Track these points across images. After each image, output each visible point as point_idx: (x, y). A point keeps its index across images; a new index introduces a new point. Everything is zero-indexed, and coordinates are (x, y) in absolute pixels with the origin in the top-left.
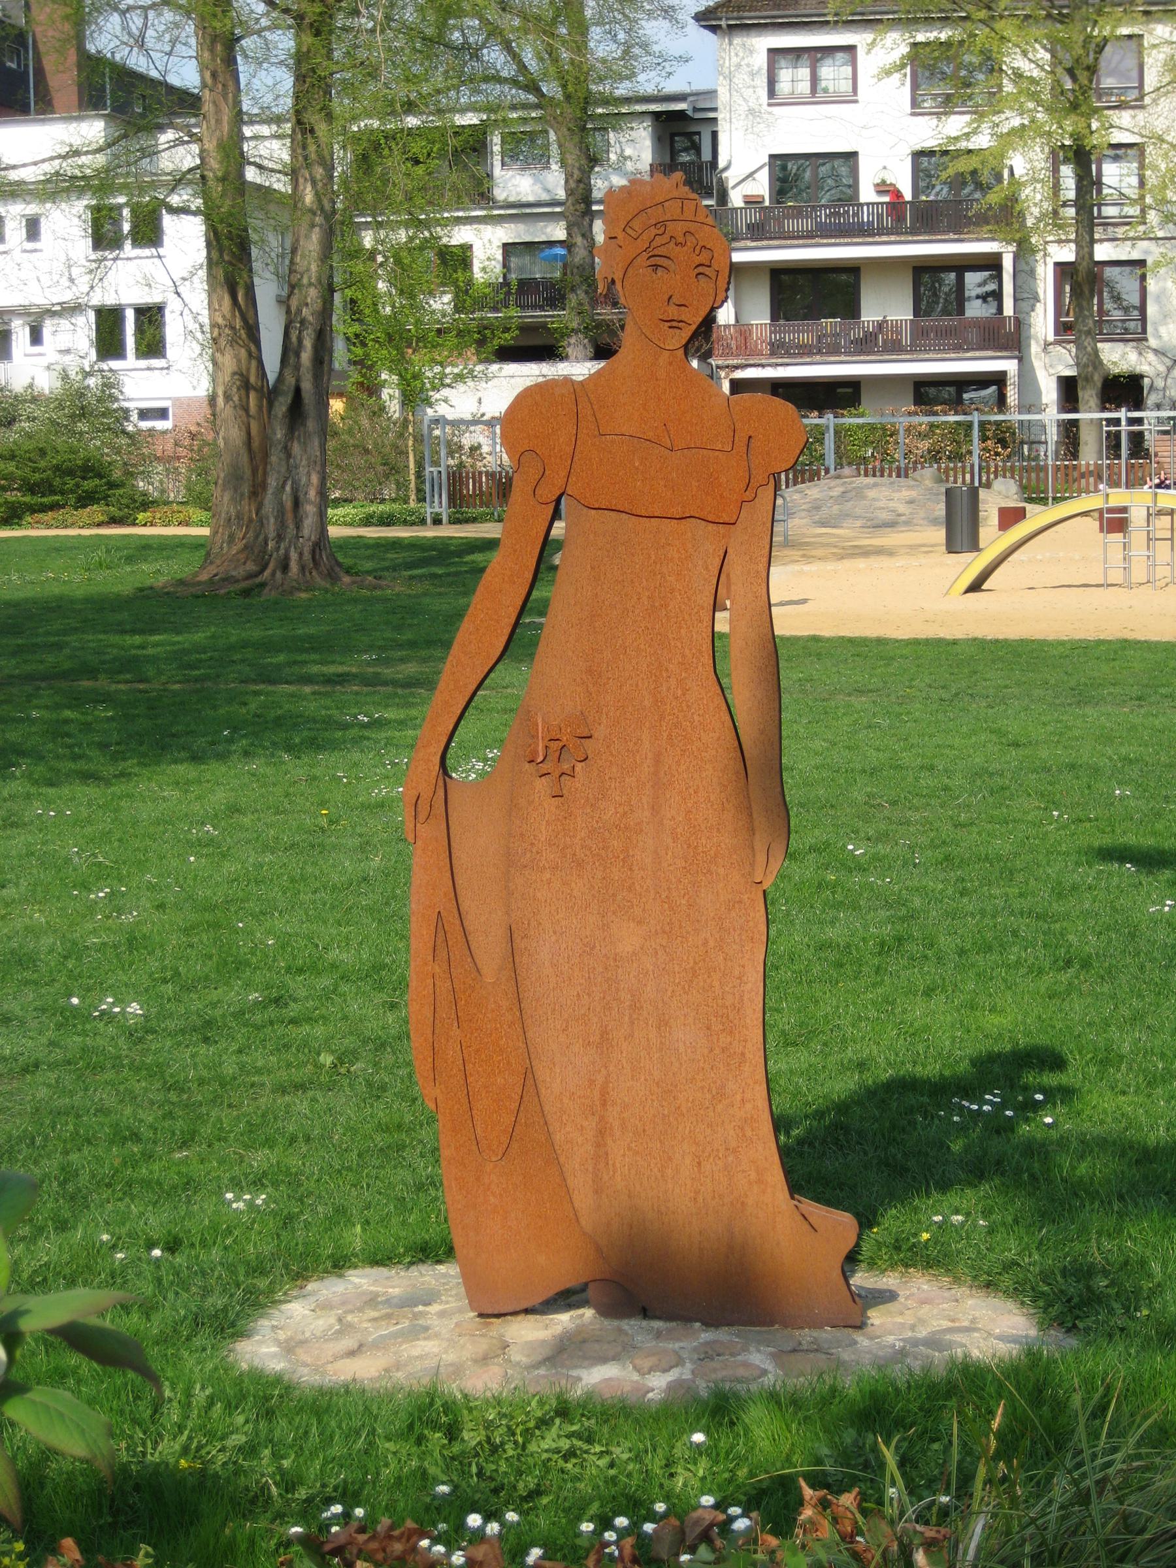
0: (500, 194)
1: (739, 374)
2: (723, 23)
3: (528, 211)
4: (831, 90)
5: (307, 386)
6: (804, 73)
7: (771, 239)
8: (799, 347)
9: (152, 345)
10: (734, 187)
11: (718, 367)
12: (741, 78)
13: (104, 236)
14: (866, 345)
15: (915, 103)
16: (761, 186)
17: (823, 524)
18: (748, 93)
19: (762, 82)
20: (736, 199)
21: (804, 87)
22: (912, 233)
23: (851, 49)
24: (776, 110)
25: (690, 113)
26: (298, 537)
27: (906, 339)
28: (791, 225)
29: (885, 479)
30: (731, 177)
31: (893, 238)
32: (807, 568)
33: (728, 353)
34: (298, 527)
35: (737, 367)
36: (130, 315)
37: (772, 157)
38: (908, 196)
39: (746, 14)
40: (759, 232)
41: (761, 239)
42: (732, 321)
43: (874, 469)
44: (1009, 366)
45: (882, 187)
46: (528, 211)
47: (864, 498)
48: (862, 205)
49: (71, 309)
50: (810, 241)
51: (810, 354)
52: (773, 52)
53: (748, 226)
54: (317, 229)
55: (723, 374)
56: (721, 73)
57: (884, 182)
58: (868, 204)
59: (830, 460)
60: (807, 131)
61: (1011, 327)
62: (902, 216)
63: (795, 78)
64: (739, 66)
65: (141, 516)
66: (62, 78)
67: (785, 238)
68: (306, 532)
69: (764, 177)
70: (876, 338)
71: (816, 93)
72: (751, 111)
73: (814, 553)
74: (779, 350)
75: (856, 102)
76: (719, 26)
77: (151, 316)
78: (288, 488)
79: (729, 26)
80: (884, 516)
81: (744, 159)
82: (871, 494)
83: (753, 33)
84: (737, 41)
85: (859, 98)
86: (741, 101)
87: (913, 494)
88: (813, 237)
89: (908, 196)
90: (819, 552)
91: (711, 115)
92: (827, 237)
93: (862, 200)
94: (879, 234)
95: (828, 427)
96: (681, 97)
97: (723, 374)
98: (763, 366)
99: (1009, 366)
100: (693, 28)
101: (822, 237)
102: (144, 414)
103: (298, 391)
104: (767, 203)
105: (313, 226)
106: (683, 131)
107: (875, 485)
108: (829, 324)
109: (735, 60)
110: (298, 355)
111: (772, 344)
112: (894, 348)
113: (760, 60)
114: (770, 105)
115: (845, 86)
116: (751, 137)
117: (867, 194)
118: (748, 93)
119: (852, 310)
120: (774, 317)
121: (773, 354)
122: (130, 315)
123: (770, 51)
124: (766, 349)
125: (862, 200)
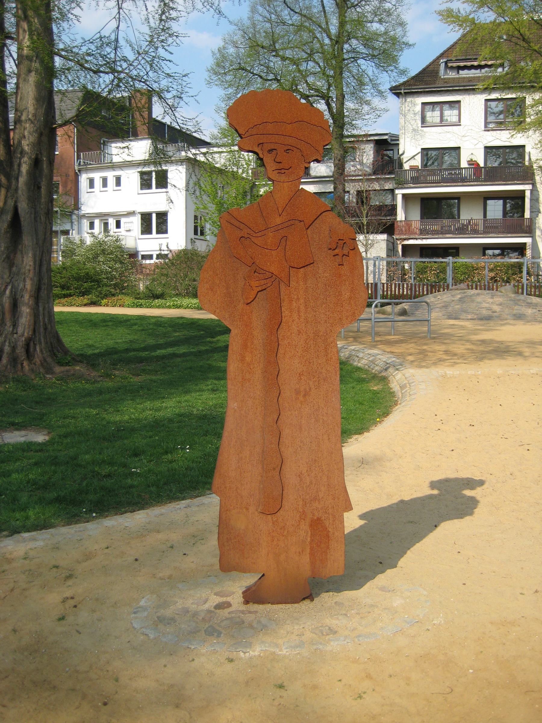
0: (313, 173)
1: (406, 242)
2: (402, 91)
3: (324, 179)
4: (449, 120)
5: (23, 206)
6: (437, 113)
7: (421, 183)
8: (433, 231)
9: (162, 228)
10: (405, 163)
11: (397, 239)
12: (410, 116)
13: (145, 184)
14: (462, 231)
15: (486, 123)
16: (418, 162)
17: (450, 317)
18: (413, 122)
19: (419, 117)
20: (406, 167)
21: (438, 120)
22: (484, 181)
23: (459, 102)
24: (425, 129)
25: (389, 140)
26: (13, 333)
27: (481, 228)
28: (430, 178)
29: (483, 291)
30: (405, 158)
31: (476, 183)
32: (450, 372)
33: (401, 233)
34: (15, 325)
35: (405, 239)
36: (154, 216)
37: (422, 149)
38: (482, 165)
39: (413, 87)
40: (416, 181)
41: (417, 184)
42: (404, 219)
43: (485, 285)
44: (528, 240)
45: (472, 163)
46: (324, 179)
47: (473, 301)
48: (462, 168)
49: (131, 214)
50: (439, 184)
51: (438, 234)
52: (424, 104)
53: (411, 178)
54: (33, 74)
55: (399, 242)
56: (401, 114)
57: (472, 160)
58: (465, 168)
59: (450, 280)
60: (437, 138)
61: (526, 223)
62: (478, 173)
63: (433, 116)
64: (409, 110)
65: (104, 301)
66: (142, 128)
67: (427, 183)
68: (20, 330)
69: (419, 158)
70: (468, 227)
71: (443, 122)
72: (414, 130)
73: (445, 341)
74: (424, 233)
75: (460, 125)
76: (401, 93)
77: (162, 217)
78: (8, 292)
79: (405, 93)
80: (485, 312)
81: (410, 152)
82: (479, 299)
83: (415, 96)
84: (409, 100)
85: (461, 123)
86: (410, 126)
87: (501, 300)
88: (440, 183)
89: (482, 165)
90: (459, 348)
91: (398, 142)
92: (446, 182)
93: (462, 166)
94: (469, 182)
95: (449, 263)
96: (386, 134)
97: (399, 242)
98: (417, 239)
99: (528, 240)
100: (392, 99)
101: (444, 182)
102: (144, 257)
103: (16, 209)
104: (420, 168)
105: (30, 71)
106: (385, 145)
107: (478, 294)
108: (446, 222)
109: (407, 108)
110: (17, 179)
111: (421, 230)
112: (475, 232)
113: (419, 108)
114: (422, 127)
115: (455, 119)
116: (413, 141)
117: (464, 164)
118: (413, 122)
119: (454, 216)
120: (422, 218)
121: (421, 234)
122: (154, 216)
123: (423, 103)
124: (418, 232)
125: (462, 166)
